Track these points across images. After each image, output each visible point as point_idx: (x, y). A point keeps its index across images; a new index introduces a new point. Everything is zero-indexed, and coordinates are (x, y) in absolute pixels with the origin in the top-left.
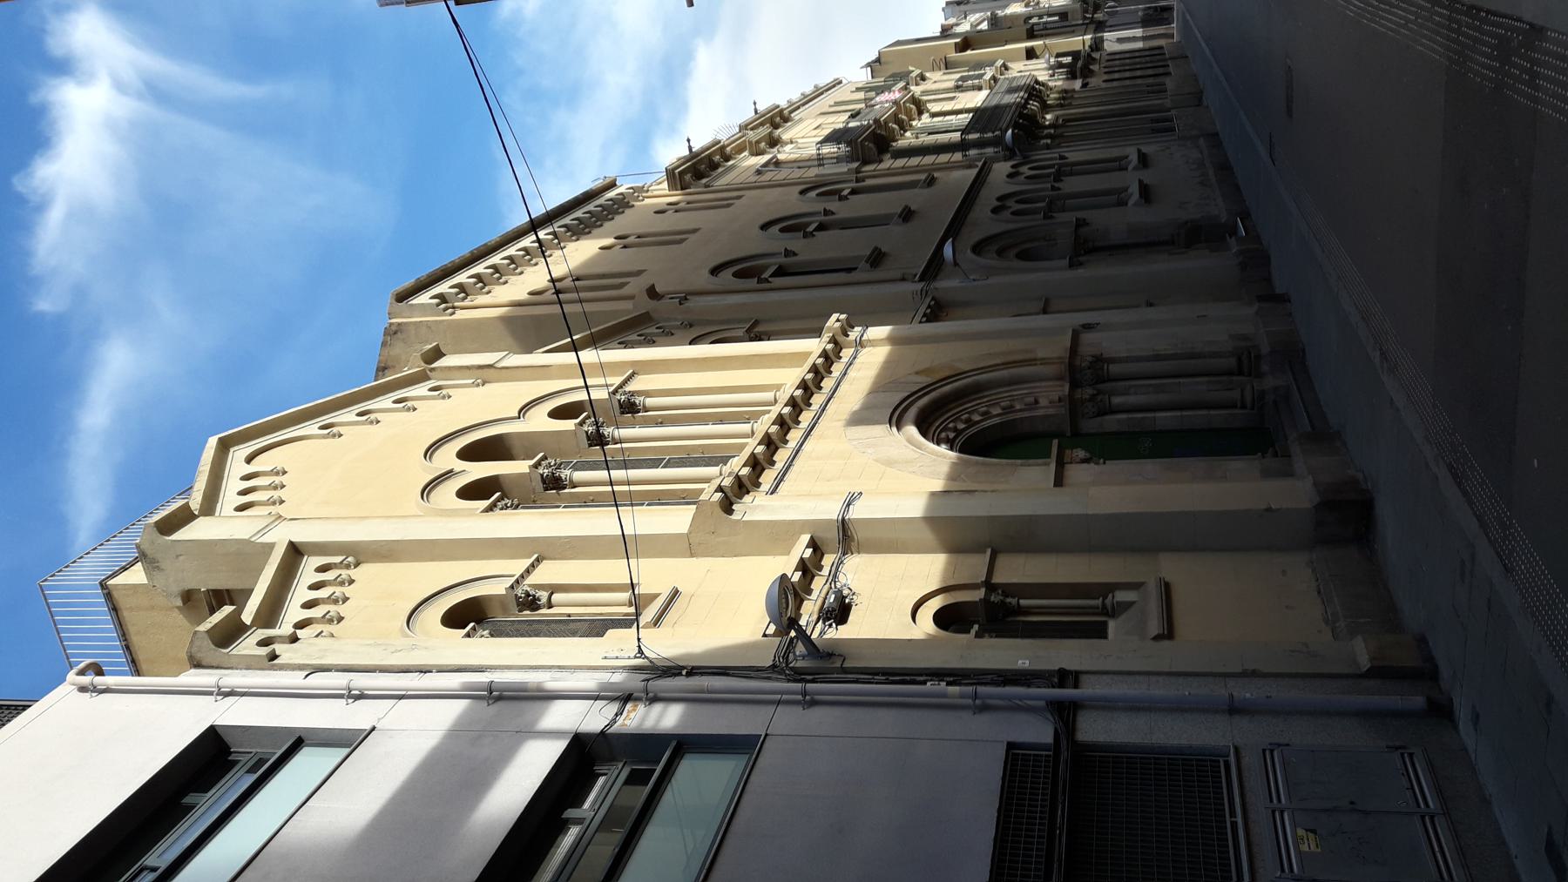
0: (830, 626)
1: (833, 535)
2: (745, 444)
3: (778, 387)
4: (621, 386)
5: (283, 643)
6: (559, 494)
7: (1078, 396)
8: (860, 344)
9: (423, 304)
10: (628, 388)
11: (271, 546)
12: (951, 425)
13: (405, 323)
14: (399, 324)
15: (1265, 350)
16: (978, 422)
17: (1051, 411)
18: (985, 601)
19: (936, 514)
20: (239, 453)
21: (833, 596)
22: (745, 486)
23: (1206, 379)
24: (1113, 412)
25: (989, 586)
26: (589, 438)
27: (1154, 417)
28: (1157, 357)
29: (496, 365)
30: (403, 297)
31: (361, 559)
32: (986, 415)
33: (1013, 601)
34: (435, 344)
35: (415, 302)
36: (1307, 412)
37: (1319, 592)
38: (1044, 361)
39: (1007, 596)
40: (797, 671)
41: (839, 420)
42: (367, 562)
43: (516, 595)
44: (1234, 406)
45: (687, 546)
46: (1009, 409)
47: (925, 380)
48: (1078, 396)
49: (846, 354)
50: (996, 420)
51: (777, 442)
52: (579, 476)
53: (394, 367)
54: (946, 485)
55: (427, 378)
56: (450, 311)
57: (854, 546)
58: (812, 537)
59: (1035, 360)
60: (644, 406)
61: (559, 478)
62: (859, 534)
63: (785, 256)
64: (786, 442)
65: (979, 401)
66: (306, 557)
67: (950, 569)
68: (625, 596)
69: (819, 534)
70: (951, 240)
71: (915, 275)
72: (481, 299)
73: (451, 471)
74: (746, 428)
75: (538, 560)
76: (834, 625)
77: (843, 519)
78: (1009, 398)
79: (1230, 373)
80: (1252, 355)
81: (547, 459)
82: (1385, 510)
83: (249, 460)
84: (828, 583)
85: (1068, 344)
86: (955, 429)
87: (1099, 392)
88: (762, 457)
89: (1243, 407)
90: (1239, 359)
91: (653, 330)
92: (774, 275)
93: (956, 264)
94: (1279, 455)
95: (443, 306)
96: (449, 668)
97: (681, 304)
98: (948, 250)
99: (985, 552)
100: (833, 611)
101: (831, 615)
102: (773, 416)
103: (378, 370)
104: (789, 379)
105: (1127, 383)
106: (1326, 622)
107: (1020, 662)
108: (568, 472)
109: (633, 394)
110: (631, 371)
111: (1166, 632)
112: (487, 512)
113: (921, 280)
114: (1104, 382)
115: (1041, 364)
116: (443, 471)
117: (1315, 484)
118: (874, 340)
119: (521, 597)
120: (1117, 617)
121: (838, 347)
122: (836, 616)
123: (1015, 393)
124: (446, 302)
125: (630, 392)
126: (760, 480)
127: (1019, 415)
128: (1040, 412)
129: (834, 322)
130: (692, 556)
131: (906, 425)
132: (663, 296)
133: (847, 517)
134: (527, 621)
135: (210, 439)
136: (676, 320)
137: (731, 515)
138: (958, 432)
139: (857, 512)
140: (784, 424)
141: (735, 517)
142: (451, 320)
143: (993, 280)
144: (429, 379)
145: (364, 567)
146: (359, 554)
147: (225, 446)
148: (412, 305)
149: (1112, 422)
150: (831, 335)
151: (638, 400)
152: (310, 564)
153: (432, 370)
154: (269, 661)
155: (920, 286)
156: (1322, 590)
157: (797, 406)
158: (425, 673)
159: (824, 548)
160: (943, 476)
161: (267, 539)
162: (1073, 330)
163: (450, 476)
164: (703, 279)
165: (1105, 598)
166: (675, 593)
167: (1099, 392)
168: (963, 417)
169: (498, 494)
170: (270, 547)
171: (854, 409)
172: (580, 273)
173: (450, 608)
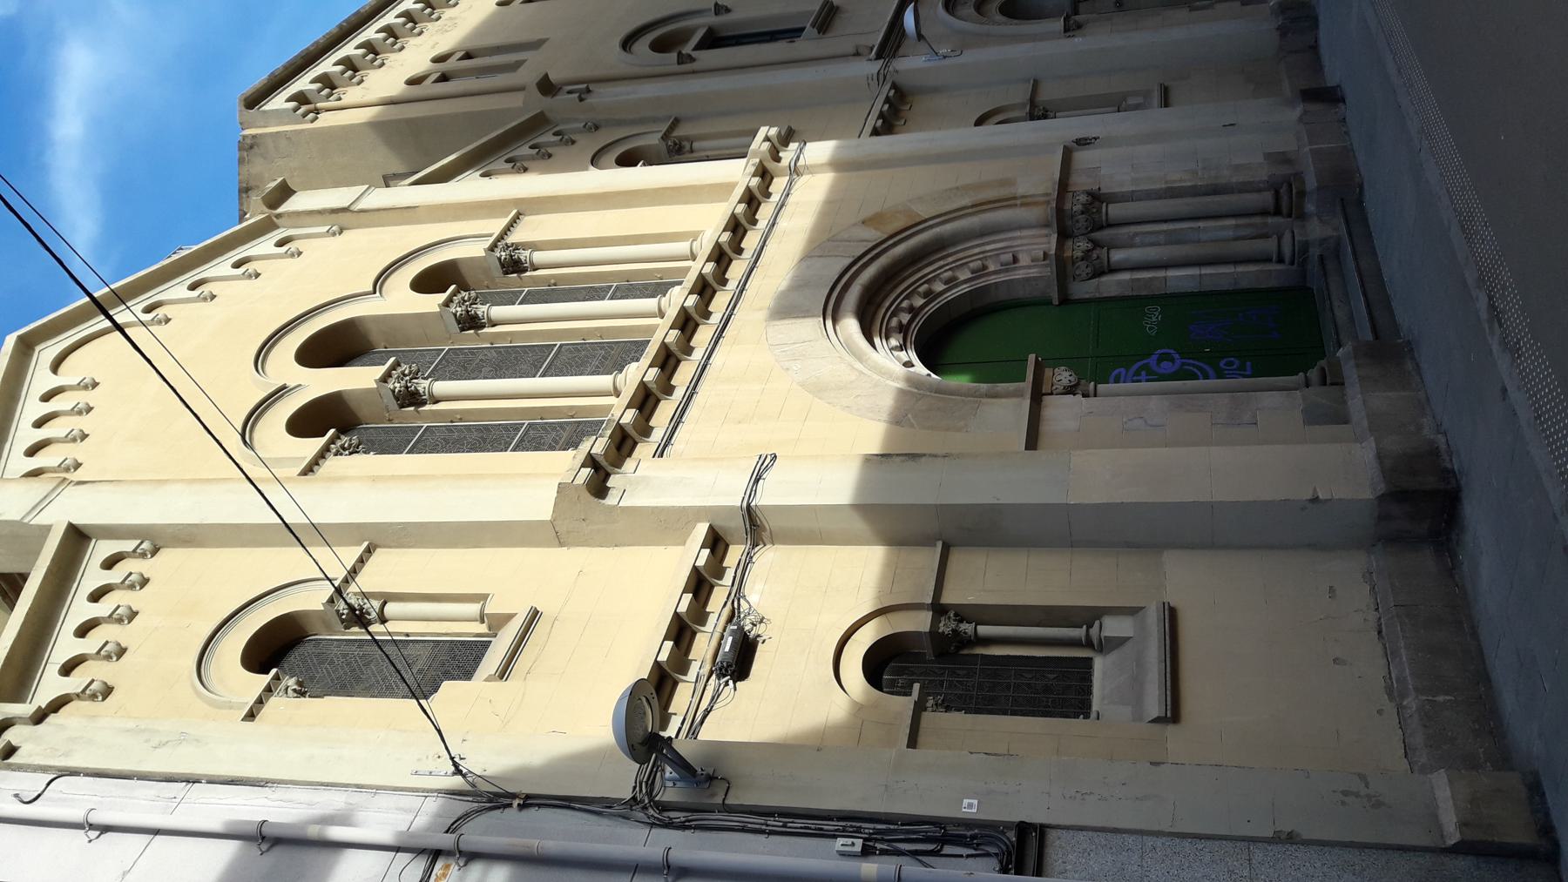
0: (727, 684)
1: (738, 524)
2: (688, 269)
3: (694, 236)
4: (501, 237)
5: (25, 724)
6: (478, 335)
7: (1068, 254)
8: (795, 171)
9: (276, 110)
10: (511, 239)
11: (48, 528)
12: (905, 304)
13: (261, 135)
14: (254, 137)
15: (1311, 183)
17: (1034, 272)
18: (933, 633)
19: (870, 501)
20: (47, 352)
21: (730, 639)
22: (629, 435)
23: (1232, 222)
24: (1113, 270)
25: (939, 609)
26: (503, 266)
27: (1165, 278)
28: (1172, 193)
29: (352, 208)
30: (254, 101)
31: (160, 544)
33: (967, 628)
34: (280, 180)
35: (266, 108)
36: (1365, 294)
37: (1380, 632)
38: (1026, 201)
39: (961, 621)
40: (663, 807)
41: (761, 309)
42: (167, 547)
43: (338, 611)
44: (1268, 260)
45: (555, 533)
46: (981, 272)
47: (873, 235)
48: (1068, 254)
49: (778, 185)
50: (964, 288)
51: (678, 354)
52: (441, 387)
53: (258, 187)
54: (889, 438)
55: (275, 227)
56: (311, 115)
57: (765, 535)
58: (711, 528)
59: (1015, 198)
60: (532, 264)
61: (416, 394)
62: (770, 523)
63: (716, 14)
64: (768, 195)
65: (942, 263)
66: (94, 540)
67: (891, 574)
69: (718, 523)
70: (913, 4)
71: (872, 49)
72: (351, 94)
73: (284, 387)
74: (650, 304)
75: (369, 551)
76: (731, 682)
77: (749, 505)
78: (981, 256)
79: (1264, 213)
80: (1294, 191)
81: (399, 365)
82: (1477, 514)
83: (55, 367)
84: (729, 603)
85: (1057, 176)
86: (911, 309)
87: (1097, 244)
88: (655, 386)
89: (1281, 260)
90: (1277, 193)
91: (548, 137)
92: (701, 46)
93: (920, 37)
94: (1328, 381)
95: (304, 108)
96: (221, 779)
97: (581, 100)
98: (909, 19)
99: (935, 545)
100: (728, 666)
101: (726, 670)
102: (691, 278)
103: (240, 191)
104: (710, 222)
105: (1133, 229)
106: (1389, 691)
107: (966, 802)
108: (527, 253)
109: (516, 247)
110: (514, 212)
111: (1169, 715)
112: (306, 474)
113: (879, 56)
114: (1101, 228)
115: (1022, 205)
116: (274, 389)
117: (1380, 457)
118: (811, 166)
119: (343, 614)
120: (1106, 654)
121: (764, 174)
122: (733, 672)
123: (988, 248)
124: (307, 102)
125: (513, 244)
126: (757, 217)
127: (993, 279)
128: (1019, 275)
129: (759, 145)
130: (561, 544)
131: (844, 316)
132: (561, 88)
133: (753, 504)
134: (356, 640)
135: (8, 338)
136: (576, 120)
137: (604, 498)
138: (914, 311)
139: (769, 496)
140: (705, 289)
141: (611, 500)
142: (314, 129)
143: (969, 56)
144: (276, 227)
145: (166, 555)
146: (154, 540)
147: (26, 347)
148: (265, 112)
149: (1111, 284)
150: (758, 160)
151: (524, 255)
152: (102, 549)
153: (279, 216)
154: (3, 760)
155: (875, 67)
156: (1384, 630)
157: (721, 257)
158: (194, 782)
159: (728, 539)
160: (885, 416)
161: (41, 519)
162: (1065, 147)
163: (282, 395)
164: (613, 59)
165: (1090, 626)
166: (534, 615)
167: (1097, 244)
168: (921, 289)
169: (453, 287)
170: (46, 530)
171: (781, 288)
172: (470, 46)
173: (255, 634)
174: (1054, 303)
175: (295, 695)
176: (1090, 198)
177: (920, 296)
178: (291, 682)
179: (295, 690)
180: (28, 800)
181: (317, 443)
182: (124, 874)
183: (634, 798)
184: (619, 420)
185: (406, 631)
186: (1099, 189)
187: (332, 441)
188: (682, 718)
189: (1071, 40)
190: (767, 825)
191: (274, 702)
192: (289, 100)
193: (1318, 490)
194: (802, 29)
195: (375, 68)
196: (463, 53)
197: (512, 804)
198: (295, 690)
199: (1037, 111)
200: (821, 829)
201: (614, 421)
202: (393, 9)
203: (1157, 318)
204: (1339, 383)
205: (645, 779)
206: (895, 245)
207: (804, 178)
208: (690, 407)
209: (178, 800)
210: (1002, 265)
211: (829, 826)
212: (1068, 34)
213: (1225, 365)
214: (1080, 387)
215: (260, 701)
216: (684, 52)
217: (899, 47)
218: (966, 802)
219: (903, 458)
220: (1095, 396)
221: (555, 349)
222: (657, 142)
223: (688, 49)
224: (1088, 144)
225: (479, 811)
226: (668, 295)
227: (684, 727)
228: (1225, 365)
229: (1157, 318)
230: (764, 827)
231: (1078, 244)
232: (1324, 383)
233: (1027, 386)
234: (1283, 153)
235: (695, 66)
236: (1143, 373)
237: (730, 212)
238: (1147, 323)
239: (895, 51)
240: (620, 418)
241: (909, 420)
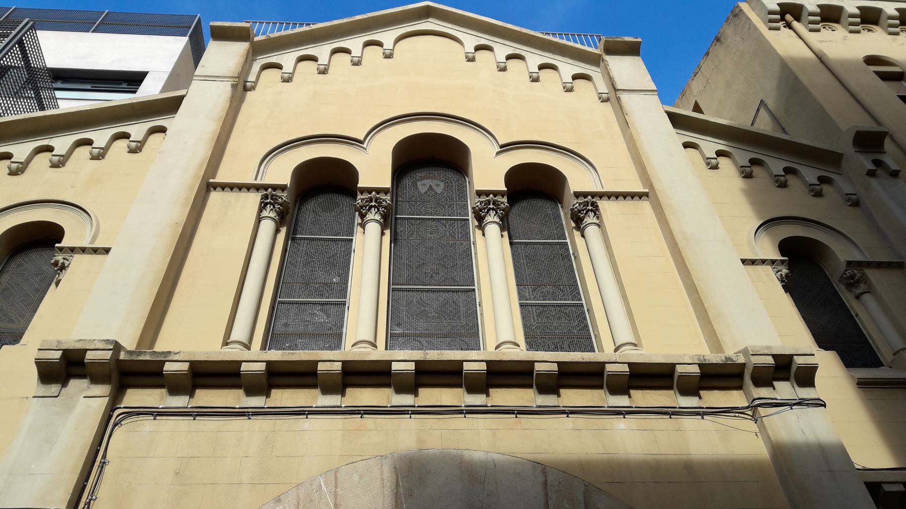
151: (590, 219)
163: (353, 144)
171: (467, 454)
175: (779, 277)
178: (785, 271)
179: (781, 275)
185: (859, 313)
191: (768, 269)
192: (897, 10)
195: (847, 30)
196: (901, 71)
198: (781, 275)
207: (751, 425)
210: (501, 148)
215: (763, 262)
222: (842, 261)
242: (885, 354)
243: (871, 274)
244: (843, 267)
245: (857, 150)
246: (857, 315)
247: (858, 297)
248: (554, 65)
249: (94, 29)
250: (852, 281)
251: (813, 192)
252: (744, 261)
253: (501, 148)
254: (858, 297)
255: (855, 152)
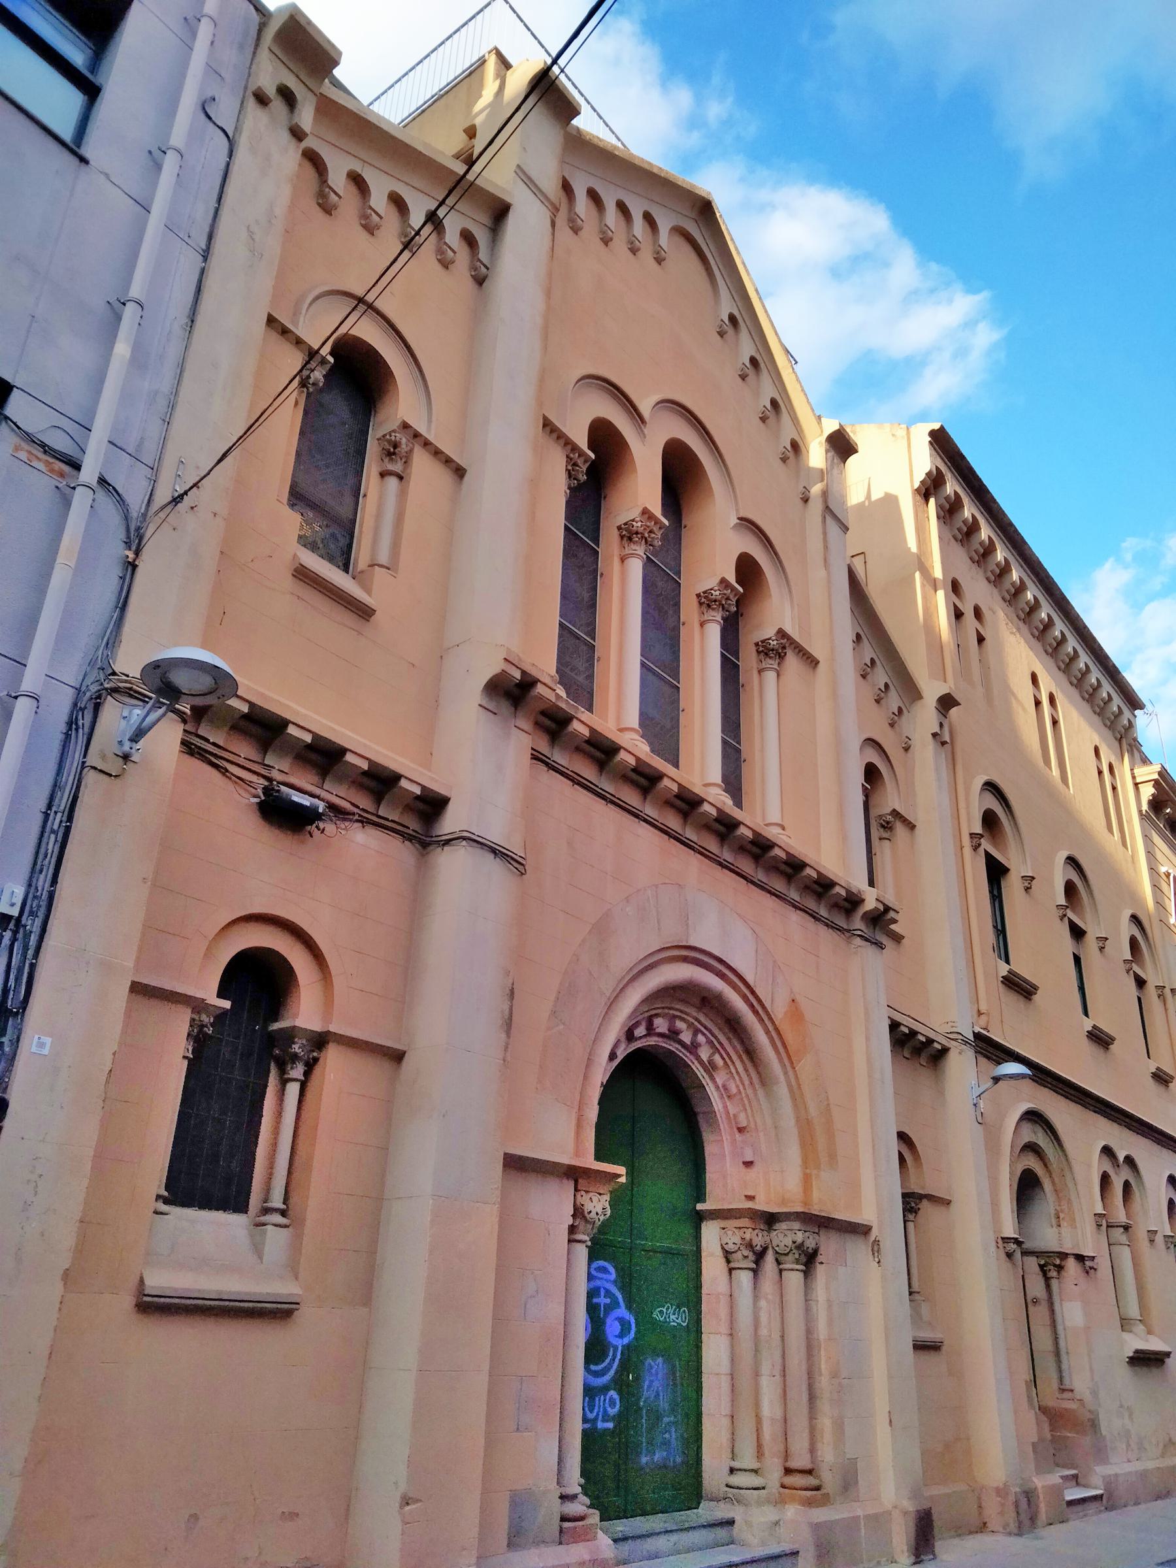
12: (701, 1038)
16: (698, 1058)
21: (308, 804)
32: (710, 1068)
68: (383, 557)
79: (787, 1455)
84: (356, 810)
93: (996, 1080)
94: (566, 1525)
107: (48, 1041)
111: (146, 1299)
125: (785, 653)
166: (364, 612)
168: (717, 1058)
169: (741, 590)
174: (698, 1205)
176: (810, 1251)
177: (709, 1057)
180: (206, 108)
181: (583, 442)
182: (107, 176)
183: (114, 673)
184: (577, 719)
185: (368, 495)
186: (822, 1263)
187: (582, 454)
188: (221, 744)
189: (994, 1244)
190: (56, 813)
193: (419, 1504)
194: (1008, 964)
197: (130, 550)
199: (912, 1203)
200: (41, 871)
201: (576, 713)
202: (1029, 576)
203: (674, 1321)
204: (563, 1537)
205: (135, 687)
206: (767, 1032)
208: (589, 794)
209: (186, 239)
210: (734, 1115)
211: (43, 881)
212: (1000, 1241)
213: (611, 1398)
214: (583, 1223)
216: (982, 840)
217: (988, 1058)
218: (48, 1041)
219: (507, 1012)
220: (570, 1241)
221: (675, 682)
223: (986, 845)
224: (873, 1254)
225: (127, 518)
226: (724, 793)
227: (210, 745)
228: (611, 1398)
229: (674, 1321)
230: (54, 809)
231: (760, 1235)
232: (564, 1519)
233: (589, 1161)
234: (857, 1482)
235: (968, 850)
236: (608, 1301)
237: (807, 861)
238: (667, 1309)
239: (981, 1053)
240: (580, 721)
241: (557, 1026)
242: (361, 555)
243: (421, 461)
244: (395, 425)
245: (484, 703)
246: (365, 496)
247: (383, 475)
248: (324, 164)
249: (592, 639)
250: (392, 450)
251: (475, 271)
252: (271, 321)
253: (734, 1115)
254: (383, 475)
255: (480, 705)
